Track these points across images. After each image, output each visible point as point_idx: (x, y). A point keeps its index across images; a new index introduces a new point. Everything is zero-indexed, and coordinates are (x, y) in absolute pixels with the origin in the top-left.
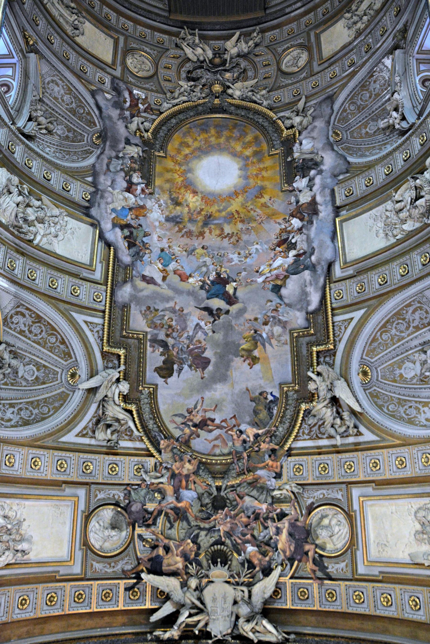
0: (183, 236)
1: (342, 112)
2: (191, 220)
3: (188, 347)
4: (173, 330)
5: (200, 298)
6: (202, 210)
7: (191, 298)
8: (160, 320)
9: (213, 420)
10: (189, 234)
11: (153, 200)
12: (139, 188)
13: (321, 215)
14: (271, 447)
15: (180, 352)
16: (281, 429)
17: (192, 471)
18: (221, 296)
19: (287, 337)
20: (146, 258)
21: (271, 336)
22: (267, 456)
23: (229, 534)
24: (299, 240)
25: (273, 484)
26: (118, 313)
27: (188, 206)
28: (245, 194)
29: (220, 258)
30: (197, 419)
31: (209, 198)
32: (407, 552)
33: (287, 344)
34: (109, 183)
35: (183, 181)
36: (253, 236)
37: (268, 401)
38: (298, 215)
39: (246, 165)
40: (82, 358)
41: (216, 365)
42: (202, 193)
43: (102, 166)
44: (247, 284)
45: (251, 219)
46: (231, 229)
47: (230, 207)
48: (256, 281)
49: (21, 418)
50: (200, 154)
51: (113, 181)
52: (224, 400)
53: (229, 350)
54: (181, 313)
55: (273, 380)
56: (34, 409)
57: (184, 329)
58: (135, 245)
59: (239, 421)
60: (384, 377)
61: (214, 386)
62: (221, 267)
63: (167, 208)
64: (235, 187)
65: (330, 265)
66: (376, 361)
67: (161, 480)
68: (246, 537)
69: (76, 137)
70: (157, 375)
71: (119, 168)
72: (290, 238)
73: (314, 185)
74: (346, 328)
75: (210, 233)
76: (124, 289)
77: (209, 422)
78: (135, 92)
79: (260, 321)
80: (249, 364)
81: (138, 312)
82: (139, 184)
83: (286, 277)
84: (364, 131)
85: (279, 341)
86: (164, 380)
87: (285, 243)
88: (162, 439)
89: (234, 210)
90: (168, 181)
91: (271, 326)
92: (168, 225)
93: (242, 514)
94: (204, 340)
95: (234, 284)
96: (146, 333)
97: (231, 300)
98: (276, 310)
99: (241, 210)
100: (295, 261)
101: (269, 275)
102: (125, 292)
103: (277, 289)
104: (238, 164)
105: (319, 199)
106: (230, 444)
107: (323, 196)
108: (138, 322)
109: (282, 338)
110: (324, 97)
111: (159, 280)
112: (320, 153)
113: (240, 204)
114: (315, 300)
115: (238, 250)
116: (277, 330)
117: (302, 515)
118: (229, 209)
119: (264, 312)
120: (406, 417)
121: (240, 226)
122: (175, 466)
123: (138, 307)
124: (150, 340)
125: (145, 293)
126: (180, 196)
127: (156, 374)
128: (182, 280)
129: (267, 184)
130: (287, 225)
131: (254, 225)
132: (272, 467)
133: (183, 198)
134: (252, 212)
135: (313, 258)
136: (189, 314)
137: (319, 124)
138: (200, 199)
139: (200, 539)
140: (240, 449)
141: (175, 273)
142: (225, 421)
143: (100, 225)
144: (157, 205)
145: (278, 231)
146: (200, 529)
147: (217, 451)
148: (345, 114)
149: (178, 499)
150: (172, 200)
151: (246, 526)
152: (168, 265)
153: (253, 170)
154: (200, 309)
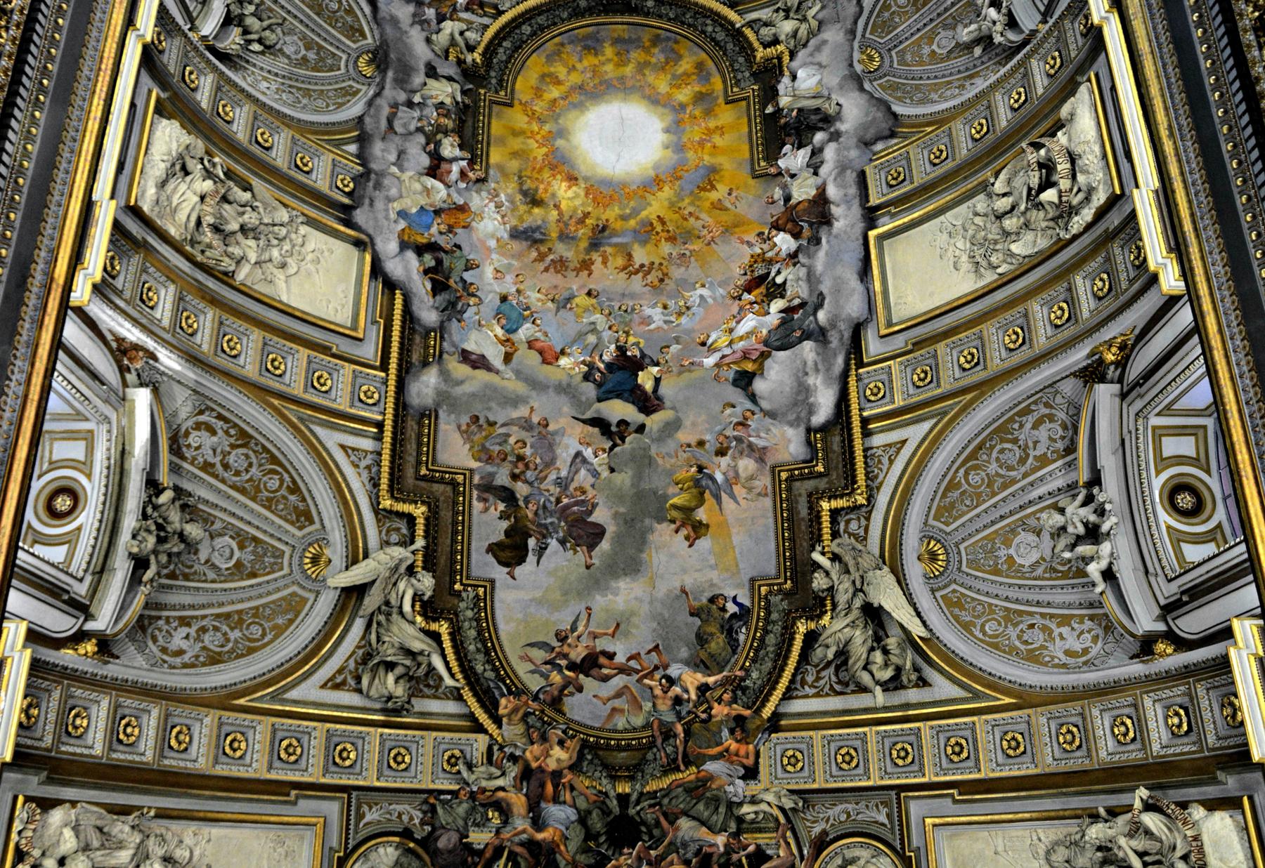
0: (546, 270)
2: (564, 237)
3: (558, 501)
4: (527, 466)
7: (563, 399)
8: (500, 444)
9: (611, 656)
10: (560, 265)
11: (484, 194)
12: (455, 168)
13: (838, 225)
14: (734, 713)
15: (540, 512)
16: (755, 675)
17: (565, 764)
18: (626, 395)
19: (765, 481)
22: (725, 733)
24: (790, 277)
25: (740, 791)
26: (410, 427)
27: (557, 206)
28: (678, 183)
29: (624, 316)
30: (578, 654)
31: (602, 191)
33: (766, 495)
34: (392, 157)
36: (694, 271)
37: (727, 615)
38: (789, 226)
39: (678, 123)
41: (619, 540)
42: (586, 179)
43: (378, 122)
44: (683, 369)
46: (648, 254)
47: (645, 209)
48: (701, 365)
50: (583, 98)
51: (401, 154)
52: (633, 614)
53: (646, 508)
54: (544, 432)
56: (232, 629)
57: (550, 464)
59: (665, 658)
61: (613, 584)
62: (627, 333)
63: (513, 210)
64: (656, 166)
65: (857, 330)
66: (956, 529)
67: (501, 782)
69: (322, 59)
71: (412, 127)
72: (773, 274)
73: (822, 162)
74: (891, 462)
75: (605, 263)
76: (424, 378)
77: (602, 660)
80: (687, 538)
81: (453, 427)
82: (455, 159)
83: (764, 356)
84: (926, 50)
85: (750, 489)
86: (506, 570)
87: (760, 284)
88: (503, 695)
90: (515, 154)
91: (734, 458)
92: (516, 246)
94: (593, 486)
96: (471, 471)
97: (648, 403)
98: (743, 424)
100: (783, 322)
101: (728, 351)
102: (426, 386)
103: (744, 381)
104: (662, 120)
105: (832, 192)
106: (648, 706)
107: (841, 186)
108: (455, 451)
109: (757, 483)
111: (497, 362)
112: (833, 96)
113: (666, 203)
114: (824, 403)
115: (664, 299)
116: (747, 465)
117: (802, 858)
118: (644, 214)
119: (718, 428)
121: (666, 248)
122: (532, 753)
123: (453, 416)
124: (478, 487)
125: (467, 388)
126: (542, 186)
127: (490, 558)
128: (545, 361)
130: (765, 247)
131: (695, 246)
132: (737, 755)
133: (546, 190)
135: (821, 315)
137: (834, 35)
138: (582, 193)
140: (670, 718)
141: (530, 347)
142: (635, 657)
143: (373, 244)
144: (492, 205)
145: (747, 260)
148: (886, 14)
149: (538, 823)
150: (525, 193)
152: (515, 330)
153: (694, 133)
154: (584, 421)
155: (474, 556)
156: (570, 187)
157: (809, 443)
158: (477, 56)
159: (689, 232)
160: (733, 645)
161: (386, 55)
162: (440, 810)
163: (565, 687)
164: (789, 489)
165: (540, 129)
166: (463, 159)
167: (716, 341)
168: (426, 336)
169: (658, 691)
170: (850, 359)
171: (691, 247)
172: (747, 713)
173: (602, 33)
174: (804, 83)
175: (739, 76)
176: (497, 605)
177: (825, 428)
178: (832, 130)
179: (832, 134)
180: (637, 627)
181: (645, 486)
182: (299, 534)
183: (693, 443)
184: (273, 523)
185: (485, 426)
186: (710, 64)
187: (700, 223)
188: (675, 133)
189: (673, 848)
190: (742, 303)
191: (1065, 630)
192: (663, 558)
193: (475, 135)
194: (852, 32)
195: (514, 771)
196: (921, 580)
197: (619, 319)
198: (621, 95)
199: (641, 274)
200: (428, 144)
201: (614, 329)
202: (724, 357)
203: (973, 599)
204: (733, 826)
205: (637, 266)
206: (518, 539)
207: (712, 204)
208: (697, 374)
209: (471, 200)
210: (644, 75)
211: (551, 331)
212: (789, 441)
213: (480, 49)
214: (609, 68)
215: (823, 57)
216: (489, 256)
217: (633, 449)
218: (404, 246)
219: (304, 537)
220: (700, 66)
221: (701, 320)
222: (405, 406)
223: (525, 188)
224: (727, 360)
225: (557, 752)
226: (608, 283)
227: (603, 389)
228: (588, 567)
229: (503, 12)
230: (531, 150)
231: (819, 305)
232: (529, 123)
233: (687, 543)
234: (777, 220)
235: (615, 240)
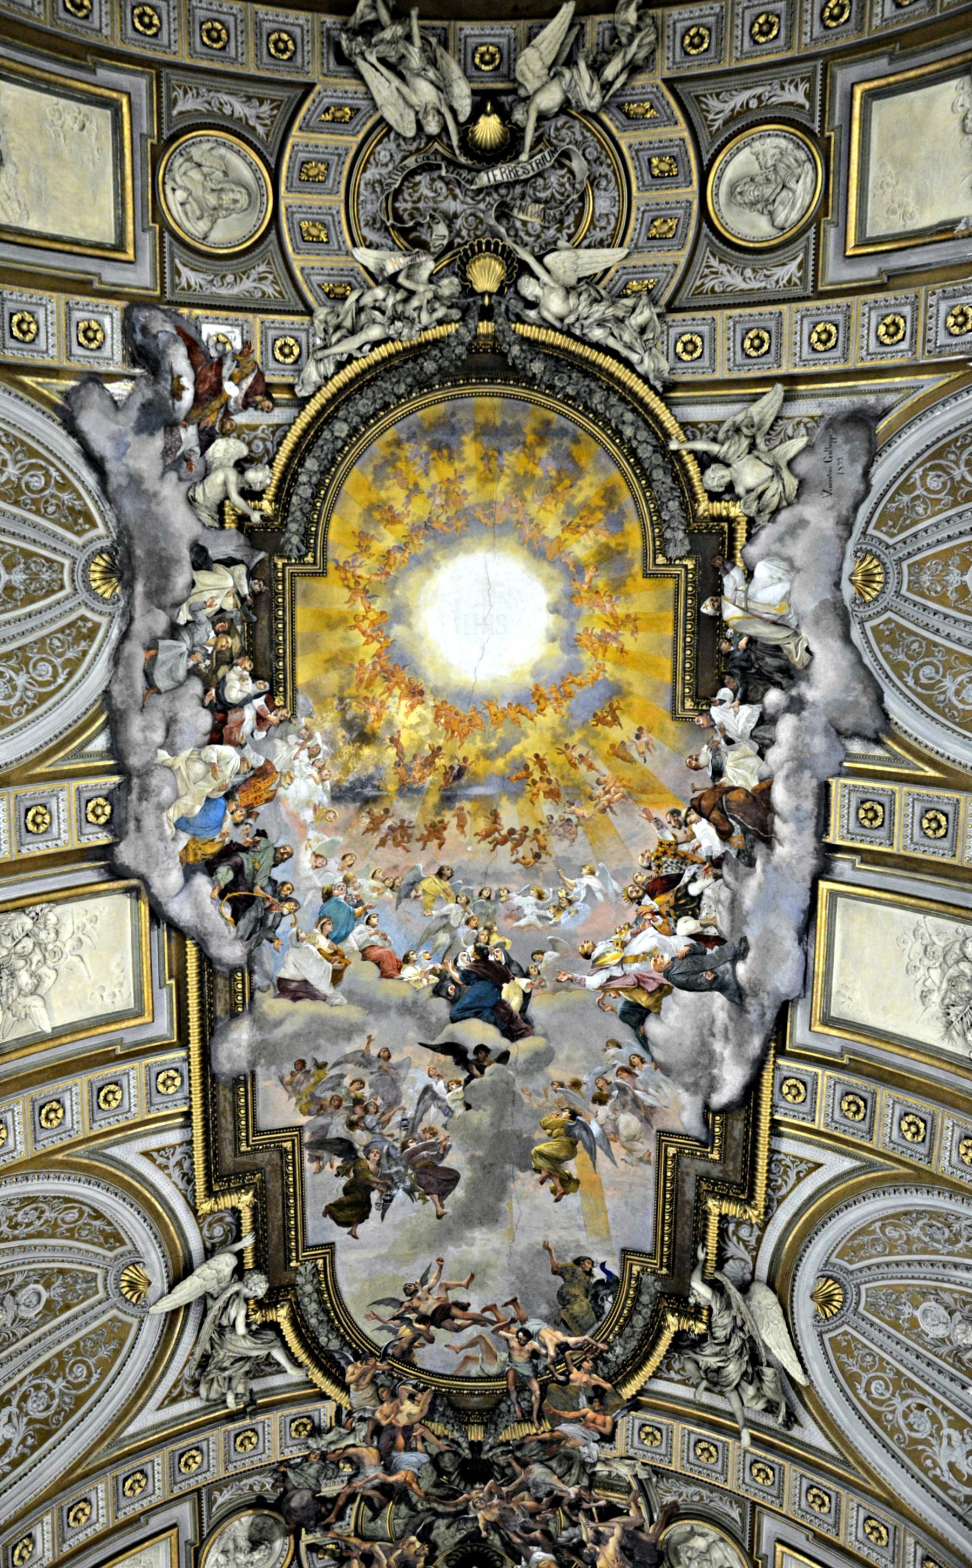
0: (383, 843)
1: (897, 492)
2: (407, 790)
3: (404, 1146)
4: (366, 1110)
5: (433, 1019)
6: (436, 752)
7: (409, 1021)
8: (333, 1089)
9: (464, 1307)
10: (401, 834)
11: (292, 739)
12: (249, 714)
13: (782, 851)
14: (594, 1383)
15: (384, 1161)
16: (618, 1350)
17: (416, 1418)
18: (487, 1013)
19: (648, 1146)
20: (285, 929)
21: (611, 1134)
22: (583, 1400)
23: (494, 1526)
24: (708, 892)
25: (595, 1453)
26: (223, 1098)
27: (394, 741)
28: (566, 704)
29: (486, 906)
30: (429, 1306)
31: (460, 711)
33: (649, 1162)
34: (158, 736)
35: (378, 655)
36: (580, 849)
37: (593, 1281)
38: (715, 815)
39: (572, 596)
40: (149, 1244)
41: (474, 1187)
42: (436, 692)
43: (131, 686)
44: (560, 987)
45: (578, 793)
46: (520, 815)
47: (518, 741)
48: (581, 983)
49: (31, 1422)
50: (430, 545)
51: (170, 724)
52: (489, 1265)
53: (507, 1152)
54: (385, 1065)
55: (609, 1238)
56: (54, 1379)
57: (393, 1104)
58: (250, 901)
59: (523, 1312)
60: (872, 1307)
61: (468, 1234)
62: (489, 930)
63: (333, 757)
64: (536, 672)
65: (784, 1010)
66: (860, 1270)
67: (350, 1441)
68: (533, 1535)
69: (34, 577)
70: (332, 1222)
71: (181, 673)
72: (685, 879)
73: (773, 742)
74: (799, 1179)
75: (461, 826)
76: (234, 1035)
77: (455, 1311)
78: (209, 331)
79: (589, 1089)
80: (554, 1191)
81: (275, 1080)
82: (248, 700)
83: (663, 991)
84: (954, 578)
85: (630, 1151)
86: (347, 1230)
87: (668, 889)
88: (349, 1363)
89: (530, 755)
90: (333, 662)
91: (614, 1110)
92: (342, 812)
93: (525, 1493)
94: (445, 1126)
95: (523, 983)
96: (300, 1128)
97: (513, 1025)
98: (628, 1071)
99: (550, 756)
100: (692, 953)
101: (617, 972)
102: (236, 1046)
103: (635, 1016)
104: (549, 589)
105: (780, 796)
106: (503, 1356)
107: (794, 791)
108: (278, 1108)
109: (638, 1146)
110: (845, 402)
111: (323, 985)
112: (804, 632)
113: (548, 736)
114: (731, 1081)
115: (539, 884)
116: (629, 1122)
117: (652, 1521)
118: (517, 749)
119: (599, 1069)
120: (906, 1432)
121: (545, 807)
122: (382, 1413)
123: (273, 1068)
124: (311, 1146)
125: (288, 1028)
126: (373, 710)
127: (329, 1221)
128: (384, 975)
129: (630, 677)
130: (680, 834)
131: (585, 810)
132: (594, 1421)
133: (379, 716)
134: (583, 768)
135: (741, 968)
136: (407, 1064)
137: (818, 515)
138: (430, 716)
139: (434, 1533)
140: (526, 1371)
141: (365, 958)
142: (491, 1308)
143: (148, 887)
144: (304, 753)
145: (653, 848)
146: (438, 1515)
147: (474, 1370)
148: (906, 498)
149: (389, 1468)
150: (349, 725)
151: (532, 1516)
152: (344, 938)
153: (594, 621)
154: (434, 1048)
155: (310, 1223)
156: (412, 707)
157: (705, 1122)
158: (267, 506)
159: (577, 787)
160: (598, 1312)
161: (130, 554)
162: (291, 1475)
163: (414, 1340)
164: (677, 1165)
165: (368, 609)
166: (258, 696)
167: (602, 955)
168: (231, 977)
169: (514, 1343)
170: (769, 1049)
171: (580, 811)
172: (607, 1386)
173: (461, 415)
174: (766, 591)
175: (668, 534)
176: (339, 1268)
177: (725, 1111)
178: (794, 692)
179: (792, 699)
180: (494, 1278)
181: (507, 1127)
182: (110, 1254)
183: (567, 1083)
184: (80, 1250)
185: (313, 1070)
186: (625, 496)
187: (593, 775)
188: (566, 617)
189: (524, 1487)
190: (641, 909)
191: (955, 1435)
192: (525, 1209)
193: (273, 644)
194: (847, 524)
195: (364, 1430)
196: (811, 1321)
197: (479, 910)
198: (488, 538)
199: (509, 845)
200: (206, 691)
201: (473, 923)
202: (611, 978)
203: (865, 1346)
204: (585, 1482)
205: (504, 832)
206: (359, 1195)
207: (612, 746)
208: (576, 995)
209: (274, 753)
210: (524, 500)
211: (390, 931)
212: (683, 1108)
213: (269, 495)
214: (470, 484)
215: (798, 550)
216: (304, 836)
217: (493, 1082)
218: (189, 872)
219: (116, 1258)
220: (609, 494)
221: (587, 922)
222: (214, 1077)
223: (349, 716)
224: (615, 984)
225: (409, 1407)
226: (466, 857)
227: (458, 1006)
228: (439, 1217)
229: (307, 400)
230: (355, 650)
231: (740, 955)
232: (351, 601)
233: (553, 1197)
234: (701, 797)
235: (477, 791)
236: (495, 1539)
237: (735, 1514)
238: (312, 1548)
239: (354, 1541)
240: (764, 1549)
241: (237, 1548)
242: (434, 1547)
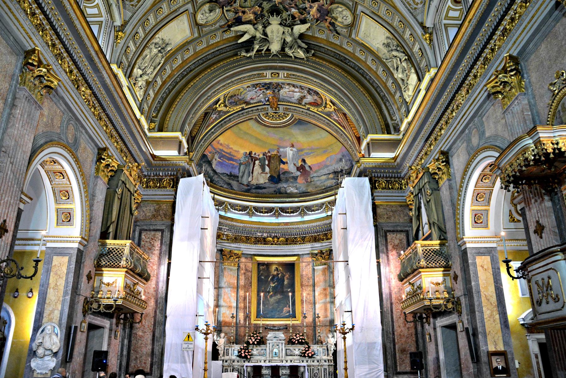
32: (377, 46)
117: (327, 4)
236: (281, 6)
237: (351, 4)
238: (227, 11)
239: (239, 8)
240: (357, 13)
241: (205, 12)
242: (263, 8)
